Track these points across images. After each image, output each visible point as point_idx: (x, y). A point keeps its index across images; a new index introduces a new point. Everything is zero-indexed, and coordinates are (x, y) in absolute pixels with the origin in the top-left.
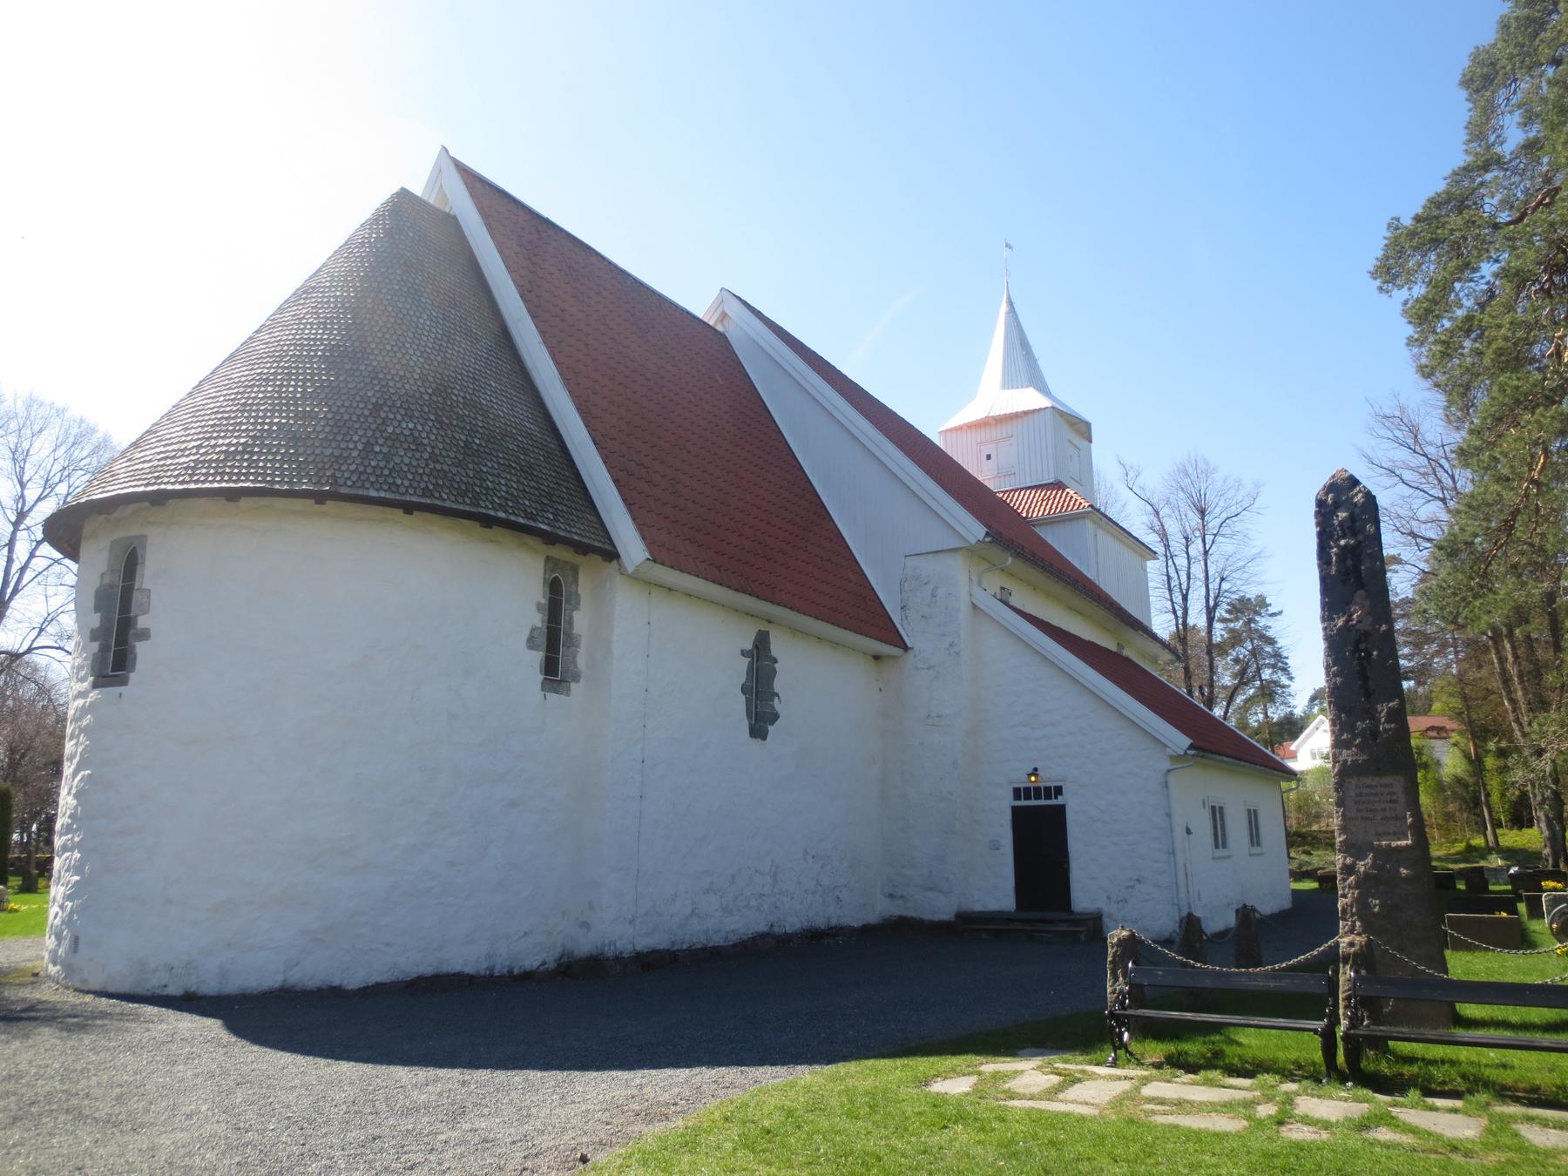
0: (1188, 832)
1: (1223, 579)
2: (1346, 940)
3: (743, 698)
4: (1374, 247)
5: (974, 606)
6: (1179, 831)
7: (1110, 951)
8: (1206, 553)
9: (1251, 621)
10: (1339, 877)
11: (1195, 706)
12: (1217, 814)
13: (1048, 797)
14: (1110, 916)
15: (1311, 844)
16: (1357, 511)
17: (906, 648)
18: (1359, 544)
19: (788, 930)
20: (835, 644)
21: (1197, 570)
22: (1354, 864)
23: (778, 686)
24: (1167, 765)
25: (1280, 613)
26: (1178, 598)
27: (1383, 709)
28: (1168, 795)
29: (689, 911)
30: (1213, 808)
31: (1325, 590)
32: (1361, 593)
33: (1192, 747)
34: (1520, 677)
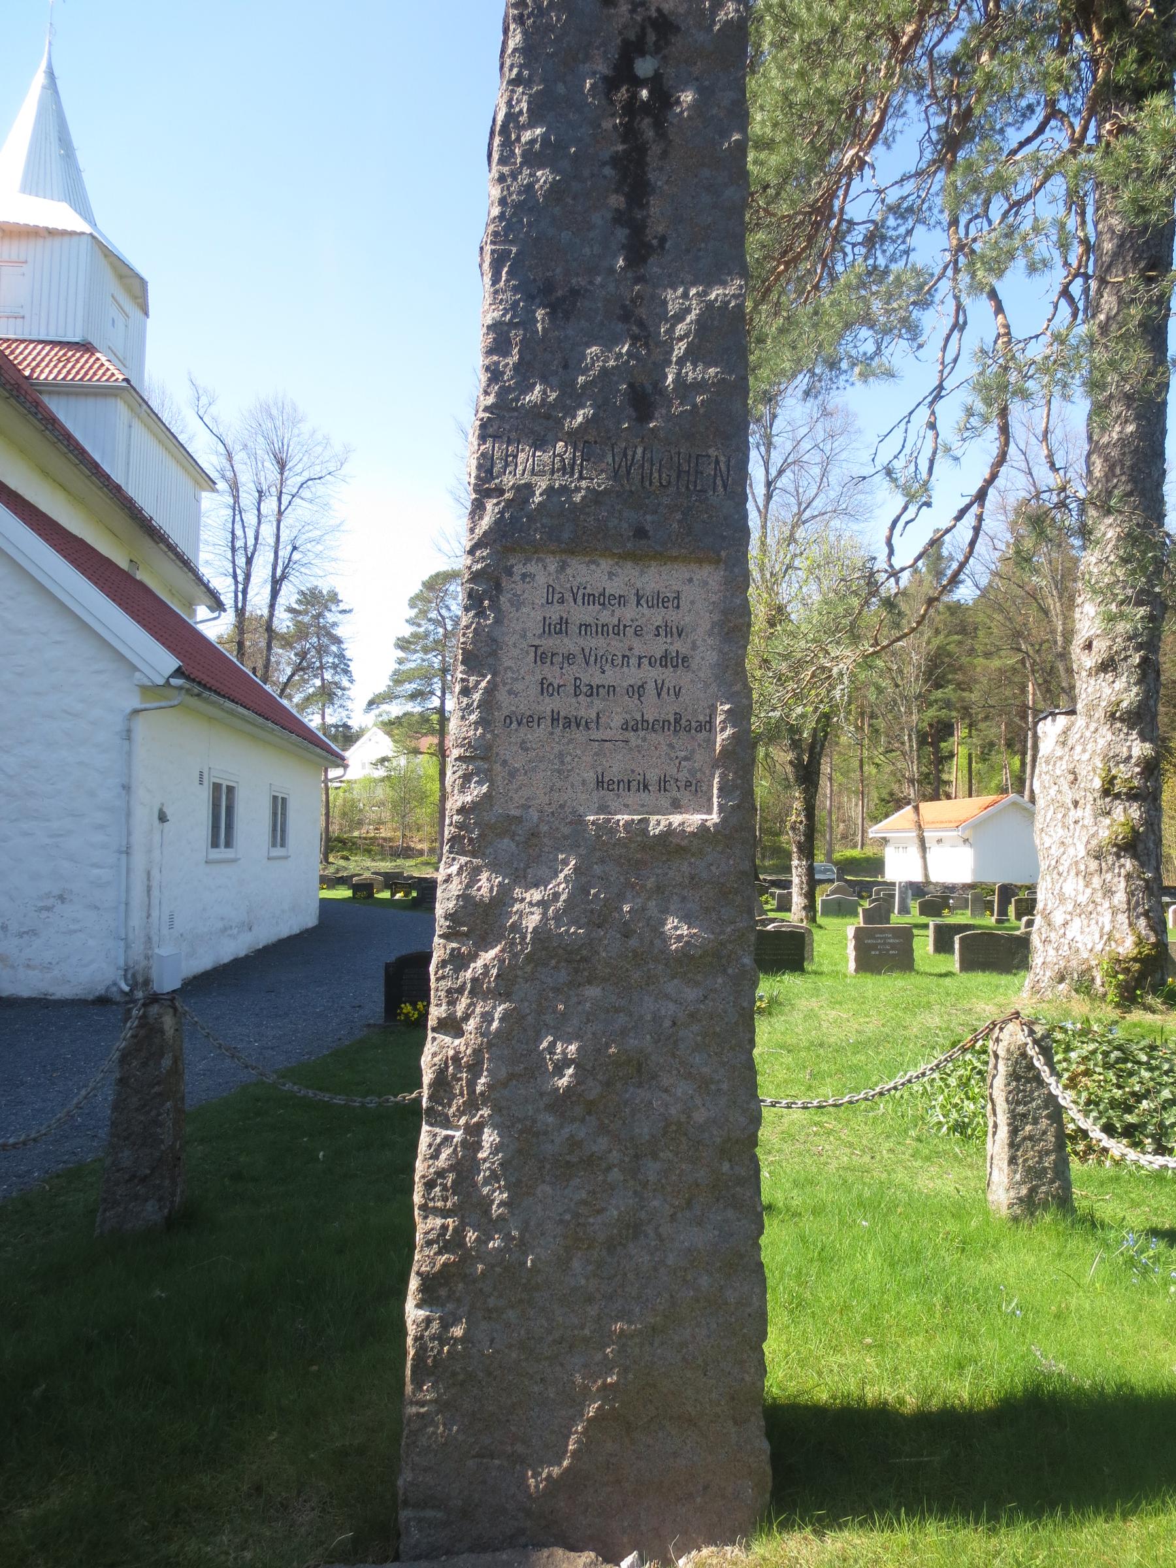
0: (163, 818)
1: (295, 548)
15: (350, 850)
21: (268, 531)
22: (502, 900)
24: (134, 701)
26: (241, 561)
27: (685, 305)
28: (129, 754)
30: (217, 787)
33: (178, 673)
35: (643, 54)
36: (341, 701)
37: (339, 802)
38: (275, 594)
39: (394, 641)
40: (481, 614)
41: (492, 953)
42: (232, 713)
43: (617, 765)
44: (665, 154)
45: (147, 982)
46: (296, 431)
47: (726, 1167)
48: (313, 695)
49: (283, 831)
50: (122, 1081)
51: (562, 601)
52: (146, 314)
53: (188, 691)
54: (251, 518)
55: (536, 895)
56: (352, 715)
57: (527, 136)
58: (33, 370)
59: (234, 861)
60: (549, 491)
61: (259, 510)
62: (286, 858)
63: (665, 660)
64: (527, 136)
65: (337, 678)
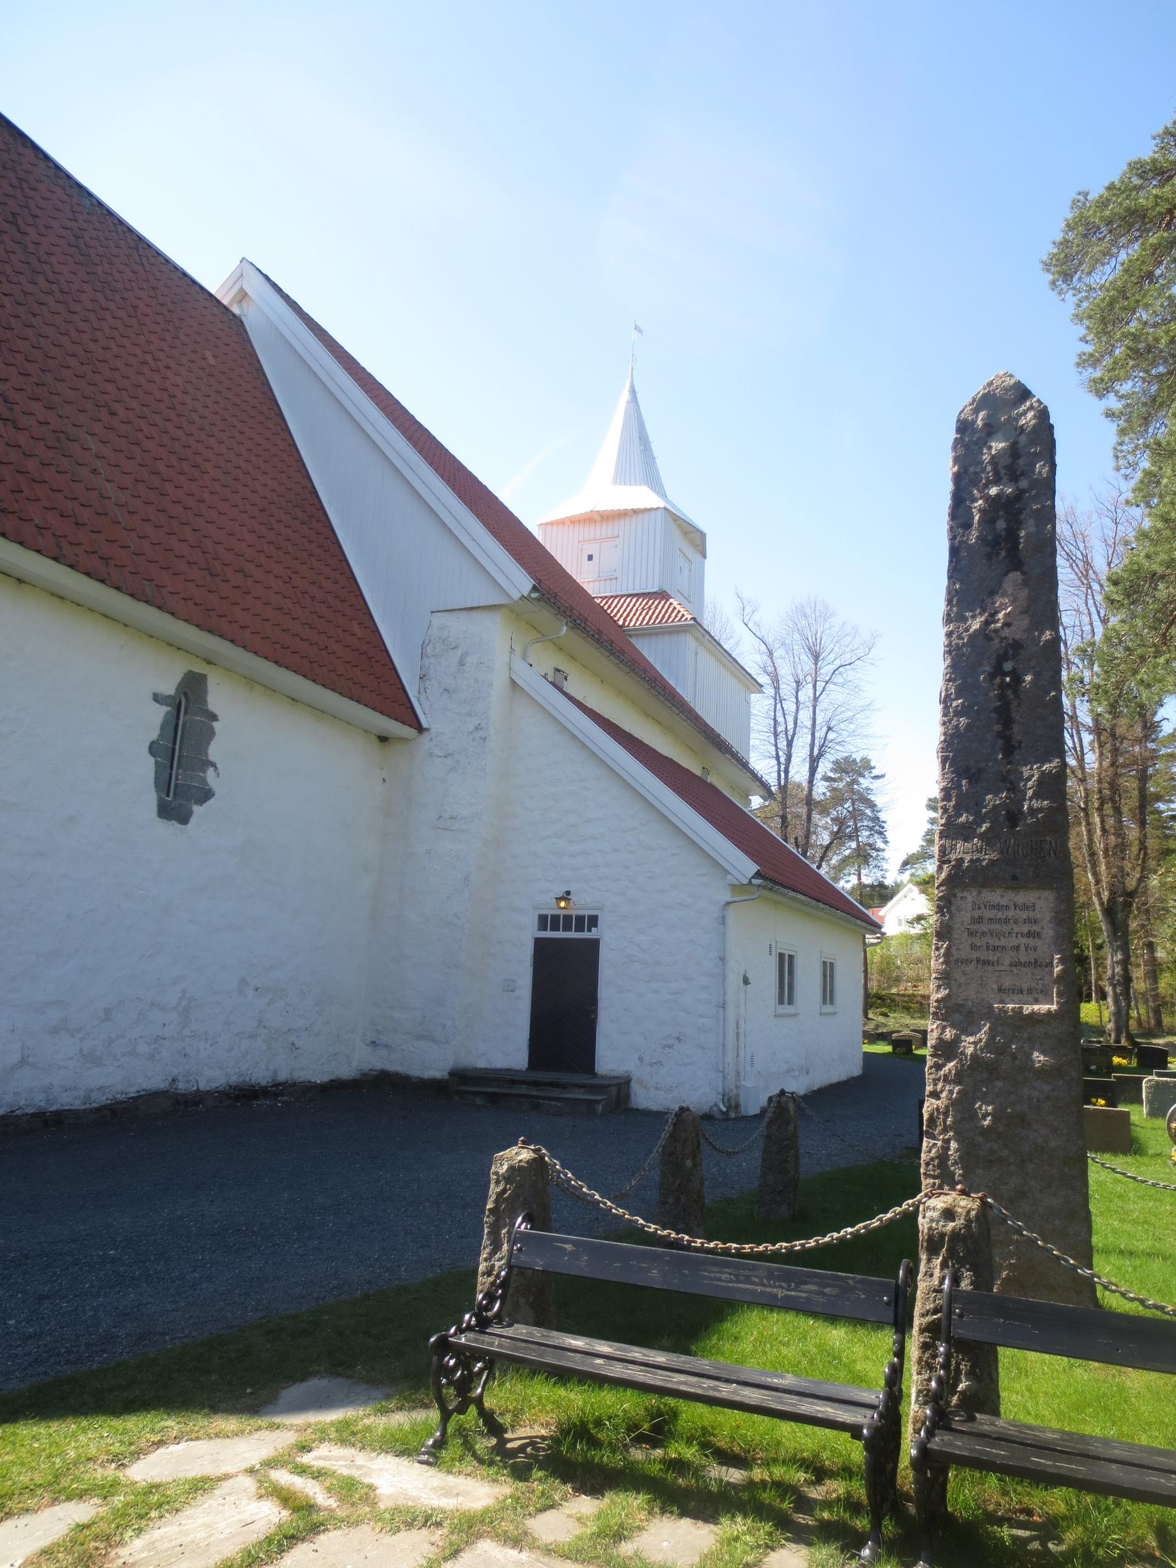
0: (746, 981)
1: (829, 729)
2: (939, 1203)
3: (151, 761)
4: (1050, 227)
5: (514, 684)
6: (734, 980)
7: (494, 1190)
8: (816, 699)
9: (854, 782)
10: (930, 1062)
11: (789, 862)
12: (786, 965)
13: (580, 928)
14: (640, 1082)
15: (889, 1007)
16: (1023, 439)
17: (420, 729)
18: (1019, 495)
19: (203, 1086)
20: (319, 712)
21: (805, 716)
22: (956, 1041)
23: (214, 752)
24: (727, 896)
25: (882, 776)
26: (782, 744)
28: (724, 934)
29: (16, 1057)
31: (955, 571)
32: (1015, 576)
33: (758, 875)
34: (1106, 850)
35: (1007, 660)
36: (876, 862)
37: (877, 959)
38: (813, 770)
39: (925, 802)
40: (943, 915)
41: (952, 1064)
42: (793, 899)
43: (1007, 982)
44: (1019, 705)
45: (737, 1106)
46: (827, 625)
47: (1067, 1170)
48: (848, 857)
49: (832, 992)
50: (768, 1137)
51: (979, 908)
52: (705, 557)
53: (764, 887)
54: (790, 706)
55: (971, 1039)
56: (887, 874)
57: (955, 704)
58: (625, 620)
59: (795, 1015)
60: (971, 861)
61: (797, 698)
62: (834, 1014)
63: (1029, 934)
64: (955, 704)
65: (871, 841)
